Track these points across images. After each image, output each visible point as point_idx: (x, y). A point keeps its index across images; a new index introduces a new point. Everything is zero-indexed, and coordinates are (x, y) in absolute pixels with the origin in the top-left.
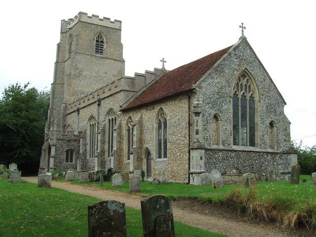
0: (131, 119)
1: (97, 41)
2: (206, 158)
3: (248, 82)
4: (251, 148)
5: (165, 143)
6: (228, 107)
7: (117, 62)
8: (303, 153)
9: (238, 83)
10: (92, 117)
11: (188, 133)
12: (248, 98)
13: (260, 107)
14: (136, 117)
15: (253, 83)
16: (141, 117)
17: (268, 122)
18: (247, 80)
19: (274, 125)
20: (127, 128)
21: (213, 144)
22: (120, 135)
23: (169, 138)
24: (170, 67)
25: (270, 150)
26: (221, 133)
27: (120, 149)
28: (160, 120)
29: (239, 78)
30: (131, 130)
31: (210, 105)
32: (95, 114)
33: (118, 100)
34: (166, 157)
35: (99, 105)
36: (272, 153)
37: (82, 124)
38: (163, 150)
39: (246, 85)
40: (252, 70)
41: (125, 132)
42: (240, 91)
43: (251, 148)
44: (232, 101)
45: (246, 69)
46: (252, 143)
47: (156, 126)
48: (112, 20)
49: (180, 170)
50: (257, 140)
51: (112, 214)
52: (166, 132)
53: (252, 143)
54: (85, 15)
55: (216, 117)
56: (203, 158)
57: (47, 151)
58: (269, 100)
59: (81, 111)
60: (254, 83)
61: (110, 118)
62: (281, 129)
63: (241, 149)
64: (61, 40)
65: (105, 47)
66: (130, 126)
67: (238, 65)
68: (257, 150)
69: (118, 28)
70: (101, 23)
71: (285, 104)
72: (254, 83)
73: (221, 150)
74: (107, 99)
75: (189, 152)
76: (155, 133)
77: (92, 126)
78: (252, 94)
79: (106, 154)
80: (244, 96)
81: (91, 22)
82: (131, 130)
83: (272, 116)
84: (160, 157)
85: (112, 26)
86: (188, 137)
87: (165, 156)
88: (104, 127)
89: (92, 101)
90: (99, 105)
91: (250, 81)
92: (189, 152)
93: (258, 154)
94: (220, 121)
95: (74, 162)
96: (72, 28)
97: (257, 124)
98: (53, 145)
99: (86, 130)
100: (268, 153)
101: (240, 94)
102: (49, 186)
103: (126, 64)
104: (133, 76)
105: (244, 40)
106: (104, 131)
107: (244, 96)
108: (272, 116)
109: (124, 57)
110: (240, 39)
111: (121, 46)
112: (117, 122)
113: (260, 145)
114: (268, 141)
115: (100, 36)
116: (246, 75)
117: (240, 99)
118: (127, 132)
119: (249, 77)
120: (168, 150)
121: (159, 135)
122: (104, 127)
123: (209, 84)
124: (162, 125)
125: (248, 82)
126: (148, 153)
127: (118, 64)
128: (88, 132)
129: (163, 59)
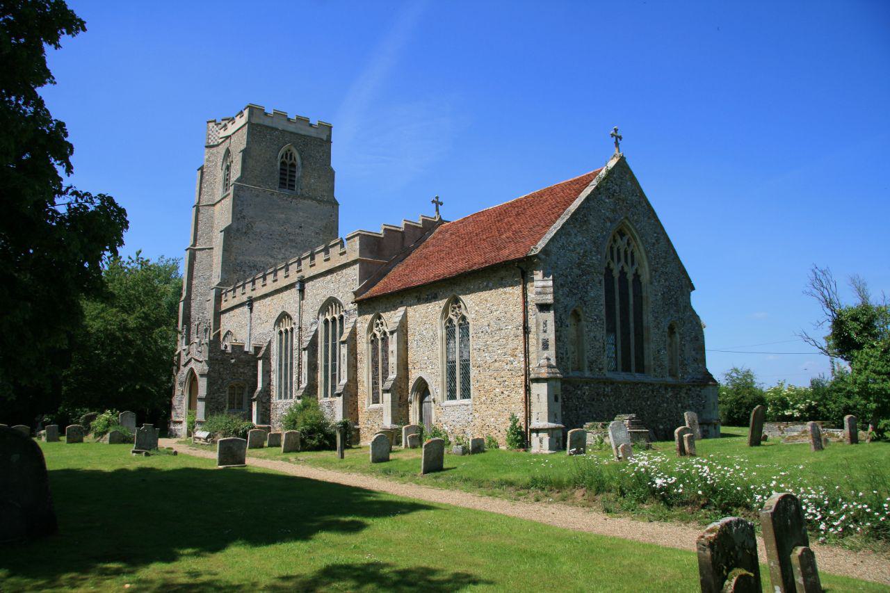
1: (283, 163)
2: (563, 399)
3: (629, 244)
6: (597, 293)
8: (69, 366)
9: (612, 248)
10: (284, 316)
11: (521, 348)
12: (630, 277)
13: (652, 294)
15: (638, 246)
16: (405, 316)
17: (665, 325)
18: (628, 240)
19: (676, 330)
22: (353, 353)
23: (475, 358)
25: (669, 379)
28: (450, 321)
31: (566, 290)
32: (293, 310)
34: (469, 397)
35: (302, 291)
36: (673, 387)
37: (258, 331)
39: (626, 252)
41: (363, 346)
43: (638, 377)
44: (603, 282)
45: (626, 218)
46: (641, 368)
47: (441, 332)
50: (649, 360)
51: (872, 585)
53: (641, 368)
55: (576, 314)
56: (560, 400)
58: (666, 280)
59: (256, 305)
60: (641, 247)
62: (687, 338)
65: (298, 174)
67: (614, 211)
70: (291, 128)
75: (528, 390)
76: (439, 347)
77: (285, 335)
78: (637, 270)
80: (623, 274)
83: (672, 312)
84: (452, 396)
87: (466, 394)
88: (315, 336)
90: (302, 291)
91: (633, 243)
92: (528, 390)
93: (650, 387)
94: (583, 323)
96: (230, 136)
107: (623, 274)
108: (672, 312)
109: (337, 195)
111: (329, 175)
112: (345, 326)
113: (655, 370)
114: (666, 363)
116: (626, 230)
119: (632, 235)
120: (471, 383)
122: (315, 336)
123: (563, 247)
125: (629, 244)
126: (423, 389)
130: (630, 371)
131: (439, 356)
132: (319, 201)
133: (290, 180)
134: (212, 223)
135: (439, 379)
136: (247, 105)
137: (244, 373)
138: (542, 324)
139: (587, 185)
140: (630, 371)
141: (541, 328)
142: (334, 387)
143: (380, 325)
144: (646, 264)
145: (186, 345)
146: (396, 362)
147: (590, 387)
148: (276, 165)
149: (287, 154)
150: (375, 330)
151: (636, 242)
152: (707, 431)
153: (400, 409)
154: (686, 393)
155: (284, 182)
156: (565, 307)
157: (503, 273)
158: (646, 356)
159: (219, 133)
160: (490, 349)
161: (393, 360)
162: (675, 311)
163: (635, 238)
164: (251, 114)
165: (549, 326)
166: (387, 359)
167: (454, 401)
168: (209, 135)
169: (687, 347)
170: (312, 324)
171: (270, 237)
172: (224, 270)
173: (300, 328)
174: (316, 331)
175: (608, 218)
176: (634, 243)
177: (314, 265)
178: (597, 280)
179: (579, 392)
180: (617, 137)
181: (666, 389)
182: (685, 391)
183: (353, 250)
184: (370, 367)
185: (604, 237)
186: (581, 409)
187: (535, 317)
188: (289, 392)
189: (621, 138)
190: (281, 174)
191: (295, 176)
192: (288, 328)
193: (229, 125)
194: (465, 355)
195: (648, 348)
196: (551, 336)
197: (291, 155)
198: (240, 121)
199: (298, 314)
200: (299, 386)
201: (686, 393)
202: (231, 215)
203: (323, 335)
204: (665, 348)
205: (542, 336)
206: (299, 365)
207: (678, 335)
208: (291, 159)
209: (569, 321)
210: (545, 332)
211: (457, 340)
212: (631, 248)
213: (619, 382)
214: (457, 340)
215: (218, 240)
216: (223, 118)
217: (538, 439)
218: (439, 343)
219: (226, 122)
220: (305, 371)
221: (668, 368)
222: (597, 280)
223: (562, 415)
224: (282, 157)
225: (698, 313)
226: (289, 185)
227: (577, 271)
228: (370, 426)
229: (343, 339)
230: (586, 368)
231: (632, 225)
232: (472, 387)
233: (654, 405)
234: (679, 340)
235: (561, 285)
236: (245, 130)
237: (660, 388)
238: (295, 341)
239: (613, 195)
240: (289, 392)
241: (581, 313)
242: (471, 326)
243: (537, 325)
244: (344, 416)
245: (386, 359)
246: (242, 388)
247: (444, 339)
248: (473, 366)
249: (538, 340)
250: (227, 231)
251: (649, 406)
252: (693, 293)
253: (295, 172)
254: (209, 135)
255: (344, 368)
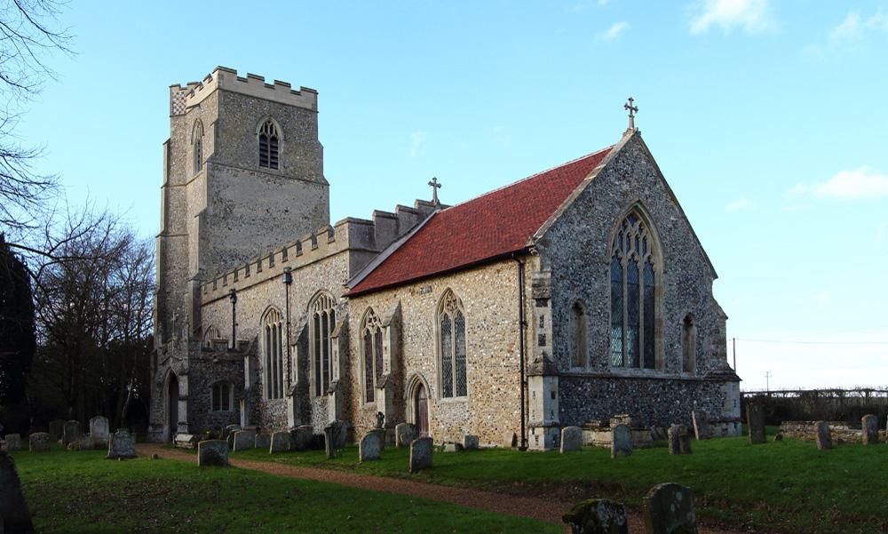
0: (372, 313)
1: (263, 137)
3: (641, 230)
4: (647, 372)
5: (461, 362)
7: (311, 187)
9: (621, 234)
11: (518, 343)
12: (641, 265)
13: (666, 284)
14: (383, 306)
18: (640, 226)
19: (694, 322)
20: (364, 333)
21: (573, 366)
23: (471, 354)
24: (454, 196)
25: (684, 375)
26: (589, 341)
27: (347, 379)
29: (624, 222)
30: (278, 329)
31: (567, 282)
32: (281, 303)
33: (337, 272)
35: (289, 282)
36: (688, 382)
38: (454, 379)
39: (637, 238)
40: (651, 205)
42: (625, 251)
43: (647, 372)
44: (609, 273)
45: (639, 201)
46: (651, 363)
48: (296, 88)
49: (501, 420)
50: (660, 355)
52: (463, 341)
53: (651, 363)
54: (260, 82)
55: (577, 308)
57: (166, 389)
58: (683, 268)
60: (655, 234)
61: (320, 313)
63: (628, 375)
64: (173, 133)
65: (281, 151)
66: (370, 329)
68: (659, 376)
69: (310, 107)
70: (270, 95)
71: (716, 277)
72: (655, 234)
73: (589, 378)
74: (308, 270)
75: (524, 384)
78: (649, 258)
79: (312, 390)
80: (632, 260)
81: (246, 93)
82: (278, 329)
83: (689, 303)
84: (448, 394)
85: (294, 100)
86: (518, 351)
87: (462, 391)
88: (305, 332)
89: (272, 273)
90: (289, 282)
92: (524, 384)
93: (661, 383)
94: (586, 317)
95: (231, 409)
96: (199, 105)
97: (660, 320)
98: (182, 374)
99: (256, 339)
100: (680, 382)
101: (625, 257)
102: (228, 465)
103: (331, 189)
104: (370, 217)
105: (636, 137)
106: (303, 341)
107: (632, 260)
108: (689, 303)
110: (625, 134)
111: (316, 151)
114: (680, 358)
115: (267, 126)
116: (639, 216)
117: (641, 270)
118: (363, 341)
119: (645, 219)
121: (443, 345)
122: (305, 332)
123: (564, 236)
124: (452, 325)
125: (641, 230)
127: (313, 190)
128: (262, 343)
129: (435, 179)
130: (639, 367)
131: (435, 352)
132: (307, 182)
133: (272, 157)
134: (186, 205)
135: (435, 376)
136: (214, 68)
137: (229, 372)
138: (538, 319)
139: (589, 171)
140: (639, 367)
141: (538, 322)
142: (326, 385)
143: (373, 321)
144: (660, 251)
145: (163, 343)
146: (389, 359)
147: (593, 383)
148: (255, 140)
149: (266, 127)
150: (368, 326)
151: (649, 228)
152: (726, 429)
153: (396, 401)
154: (704, 390)
155: (264, 159)
156: (566, 300)
157: (499, 266)
158: (656, 350)
159: (185, 101)
160: (486, 345)
161: (387, 356)
162: (692, 302)
163: (648, 223)
164: (220, 77)
165: (546, 321)
166: (381, 356)
167: (463, 397)
168: (174, 103)
169: (706, 340)
170: (301, 320)
171: (253, 222)
172: (201, 260)
173: (288, 323)
174: (306, 326)
175: (617, 202)
176: (646, 228)
177: (302, 255)
178: (602, 271)
179: (580, 389)
180: (632, 109)
181: (679, 385)
182: (702, 387)
183: (343, 241)
184: (364, 364)
185: (612, 224)
186: (581, 407)
187: (532, 311)
188: (279, 392)
189: (636, 110)
190: (261, 150)
191: (277, 153)
192: (277, 324)
193: (197, 91)
194: (461, 352)
195: (660, 342)
196: (549, 332)
197: (271, 128)
198: (210, 88)
199: (285, 309)
200: (289, 384)
201: (704, 390)
202: (206, 198)
203: (314, 331)
204: (679, 342)
205: (539, 331)
206: (289, 362)
207: (695, 328)
208: (271, 132)
209: (570, 315)
210: (542, 326)
211: (453, 335)
212: (644, 234)
213: (626, 378)
214: (453, 335)
215: (193, 225)
216: (190, 81)
217: (534, 437)
218: (434, 338)
219: (194, 86)
220: (295, 369)
221: (682, 363)
222: (602, 271)
223: (560, 412)
224: (261, 130)
225: (720, 304)
226: (272, 163)
227: (579, 262)
228: (364, 426)
229: (334, 335)
230: (588, 365)
231: (646, 210)
232: (468, 384)
233: (665, 402)
234: (696, 333)
235: (561, 276)
236: (215, 98)
237: (672, 384)
238: (284, 337)
239: (624, 176)
240: (279, 392)
241: (583, 306)
242: (466, 321)
243: (534, 319)
244: (337, 417)
245: (379, 356)
246: (226, 389)
247: (440, 335)
248: (470, 363)
249: (534, 335)
250: (203, 216)
251: (659, 403)
252: (715, 282)
253: (277, 148)
254: (174, 103)
255: (336, 365)
